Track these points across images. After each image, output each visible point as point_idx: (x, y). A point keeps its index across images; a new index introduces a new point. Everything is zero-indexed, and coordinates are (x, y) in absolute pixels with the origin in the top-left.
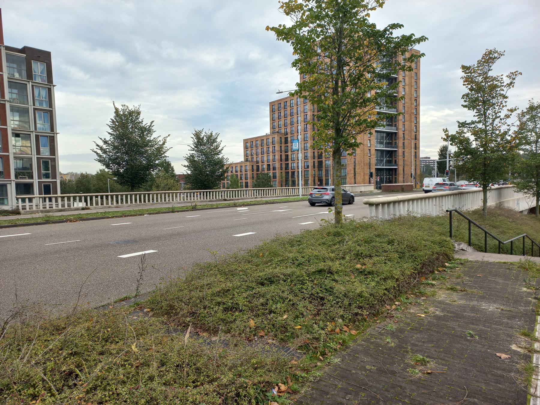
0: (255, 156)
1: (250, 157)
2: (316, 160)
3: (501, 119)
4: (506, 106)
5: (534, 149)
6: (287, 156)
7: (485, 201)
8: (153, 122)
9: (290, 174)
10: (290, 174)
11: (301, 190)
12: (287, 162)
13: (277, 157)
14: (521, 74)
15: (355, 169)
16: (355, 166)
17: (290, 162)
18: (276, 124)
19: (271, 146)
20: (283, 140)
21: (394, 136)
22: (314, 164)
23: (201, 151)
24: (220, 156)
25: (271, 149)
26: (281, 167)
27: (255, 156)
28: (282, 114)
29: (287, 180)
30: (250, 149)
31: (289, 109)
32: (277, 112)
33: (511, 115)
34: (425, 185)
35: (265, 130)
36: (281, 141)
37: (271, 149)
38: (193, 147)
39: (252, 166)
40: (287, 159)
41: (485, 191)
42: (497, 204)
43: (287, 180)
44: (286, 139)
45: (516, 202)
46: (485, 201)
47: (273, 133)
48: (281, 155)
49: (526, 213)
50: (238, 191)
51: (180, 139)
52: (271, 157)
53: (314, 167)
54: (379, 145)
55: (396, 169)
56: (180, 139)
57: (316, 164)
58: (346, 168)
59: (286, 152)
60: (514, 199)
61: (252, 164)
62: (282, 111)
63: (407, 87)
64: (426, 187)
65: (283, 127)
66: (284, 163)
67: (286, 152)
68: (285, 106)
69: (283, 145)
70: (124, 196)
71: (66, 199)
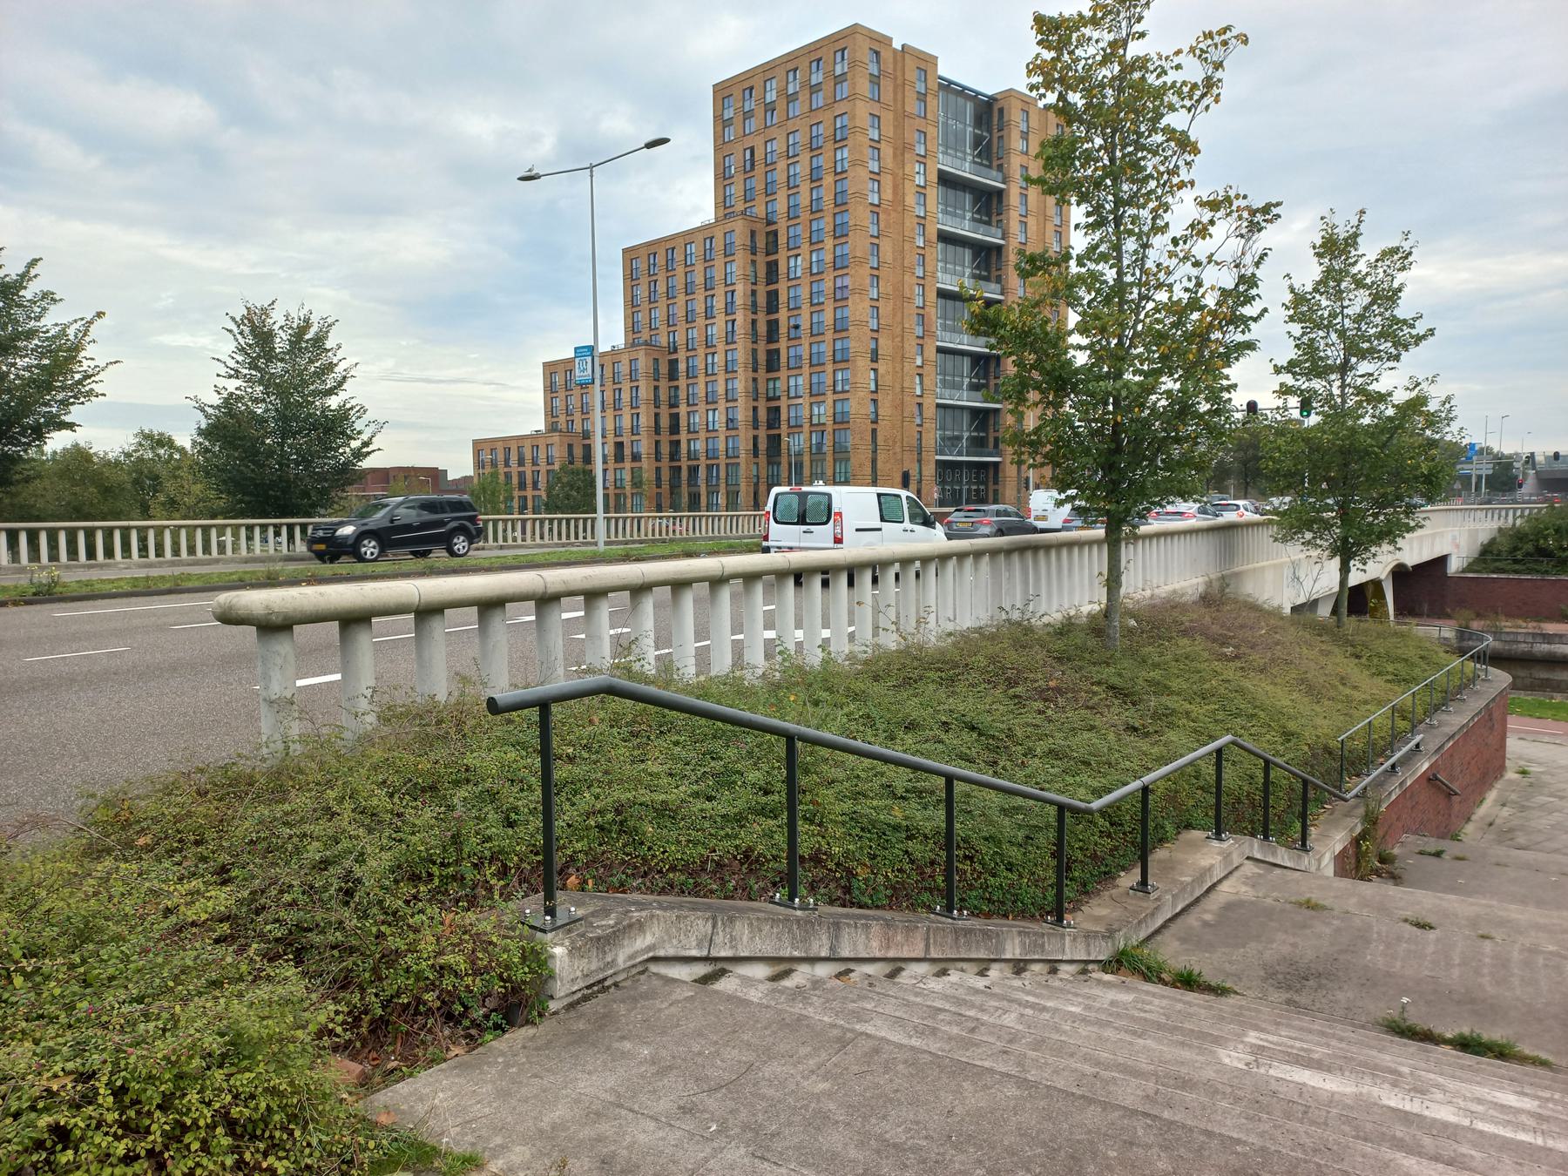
0: (577, 417)
1: (562, 419)
2: (762, 433)
3: (1175, 241)
4: (1192, 183)
5: (1336, 391)
6: (675, 418)
7: (1113, 581)
8: (34, 262)
9: (684, 474)
10: (684, 474)
11: (601, 525)
12: (675, 438)
13: (645, 421)
14: (1246, 42)
15: (874, 461)
16: (875, 452)
17: (683, 436)
18: (641, 317)
19: (626, 386)
20: (664, 369)
21: (993, 365)
22: (755, 445)
23: (267, 381)
24: (333, 402)
25: (626, 396)
26: (657, 452)
27: (577, 417)
28: (661, 288)
29: (675, 486)
30: (562, 394)
31: (680, 270)
32: (644, 280)
33: (1212, 222)
34: (1033, 514)
35: (613, 335)
36: (656, 370)
37: (626, 396)
38: (232, 364)
39: (570, 446)
40: (674, 428)
41: (1113, 541)
42: (1209, 584)
43: (675, 486)
44: (673, 364)
45: (1287, 572)
46: (1113, 581)
47: (632, 344)
48: (657, 415)
49: (1324, 611)
50: (625, 519)
51: (389, 363)
52: (626, 422)
53: (756, 455)
54: (947, 392)
55: (996, 464)
56: (389, 363)
57: (762, 446)
58: (848, 460)
59: (671, 406)
60: (1281, 565)
61: (567, 440)
62: (661, 278)
63: (1031, 221)
64: (1037, 518)
65: (663, 329)
66: (665, 438)
67: (671, 406)
68: (669, 267)
69: (664, 384)
70: (183, 533)
71: (271, 530)
